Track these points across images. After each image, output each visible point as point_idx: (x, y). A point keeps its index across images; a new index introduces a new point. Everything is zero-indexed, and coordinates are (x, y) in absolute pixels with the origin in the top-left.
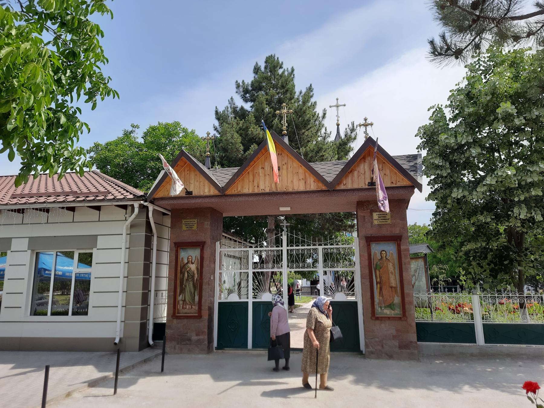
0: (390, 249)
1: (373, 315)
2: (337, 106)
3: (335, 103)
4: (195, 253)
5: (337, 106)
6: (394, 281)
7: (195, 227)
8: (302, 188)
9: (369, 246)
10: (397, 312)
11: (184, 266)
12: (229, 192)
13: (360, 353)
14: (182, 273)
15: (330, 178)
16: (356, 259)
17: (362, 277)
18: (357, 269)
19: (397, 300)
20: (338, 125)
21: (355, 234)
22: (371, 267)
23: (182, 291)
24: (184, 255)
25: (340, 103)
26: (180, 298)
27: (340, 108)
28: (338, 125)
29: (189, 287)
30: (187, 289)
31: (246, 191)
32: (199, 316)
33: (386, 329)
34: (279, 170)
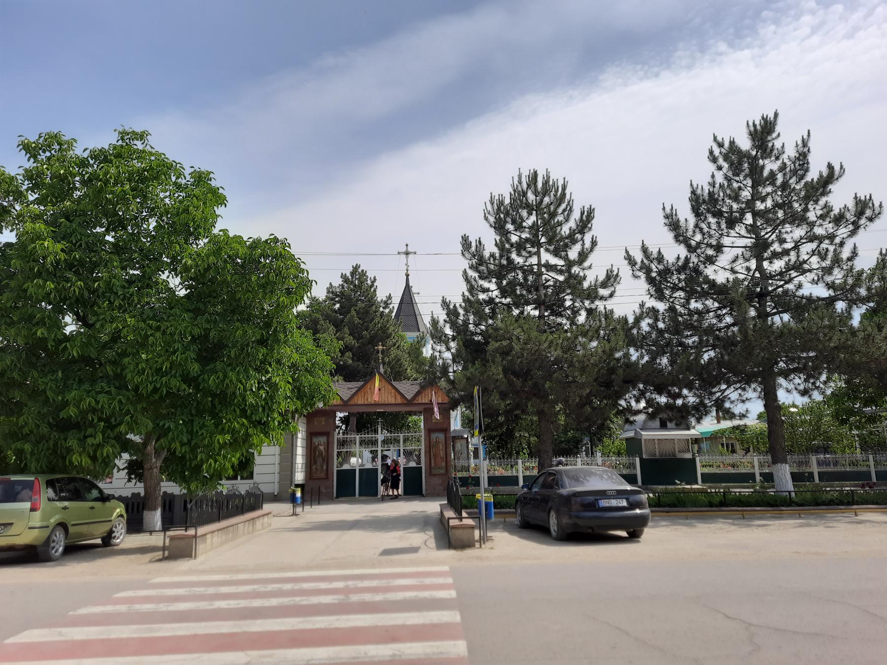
0: (441, 436)
1: (430, 473)
2: (407, 253)
3: (404, 250)
4: (323, 440)
5: (407, 253)
6: (442, 454)
7: (323, 423)
8: (393, 402)
9: (430, 435)
10: (443, 471)
11: (316, 447)
12: (352, 402)
13: (423, 496)
14: (315, 452)
15: (409, 397)
16: (423, 439)
17: (425, 452)
18: (423, 448)
19: (443, 464)
20: (407, 275)
21: (422, 417)
22: (429, 446)
23: (315, 463)
24: (316, 440)
25: (410, 250)
26: (314, 467)
27: (410, 256)
28: (407, 275)
29: (320, 460)
30: (318, 463)
31: (360, 402)
32: (327, 478)
33: (437, 481)
34: (379, 390)
